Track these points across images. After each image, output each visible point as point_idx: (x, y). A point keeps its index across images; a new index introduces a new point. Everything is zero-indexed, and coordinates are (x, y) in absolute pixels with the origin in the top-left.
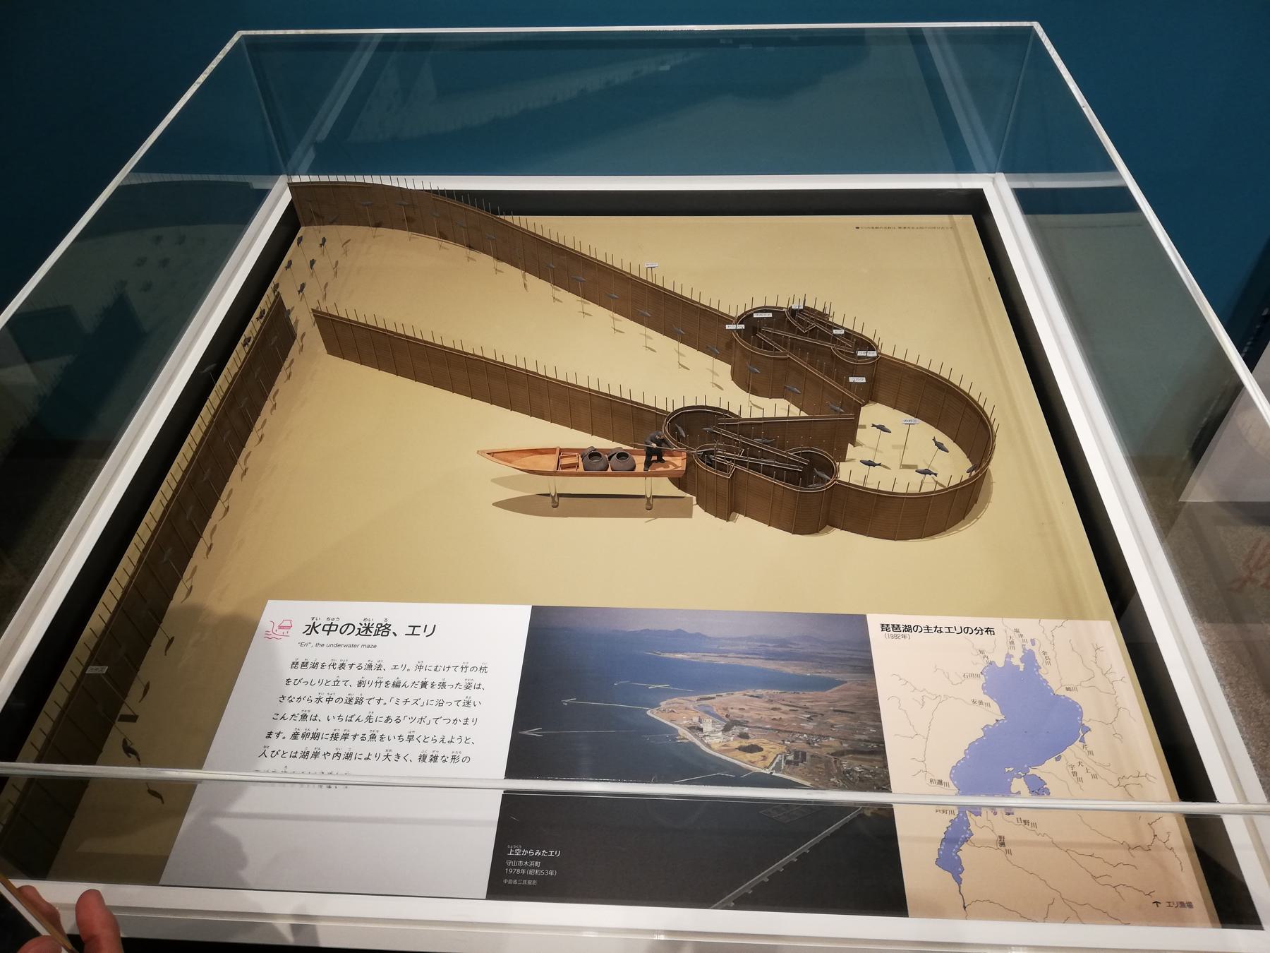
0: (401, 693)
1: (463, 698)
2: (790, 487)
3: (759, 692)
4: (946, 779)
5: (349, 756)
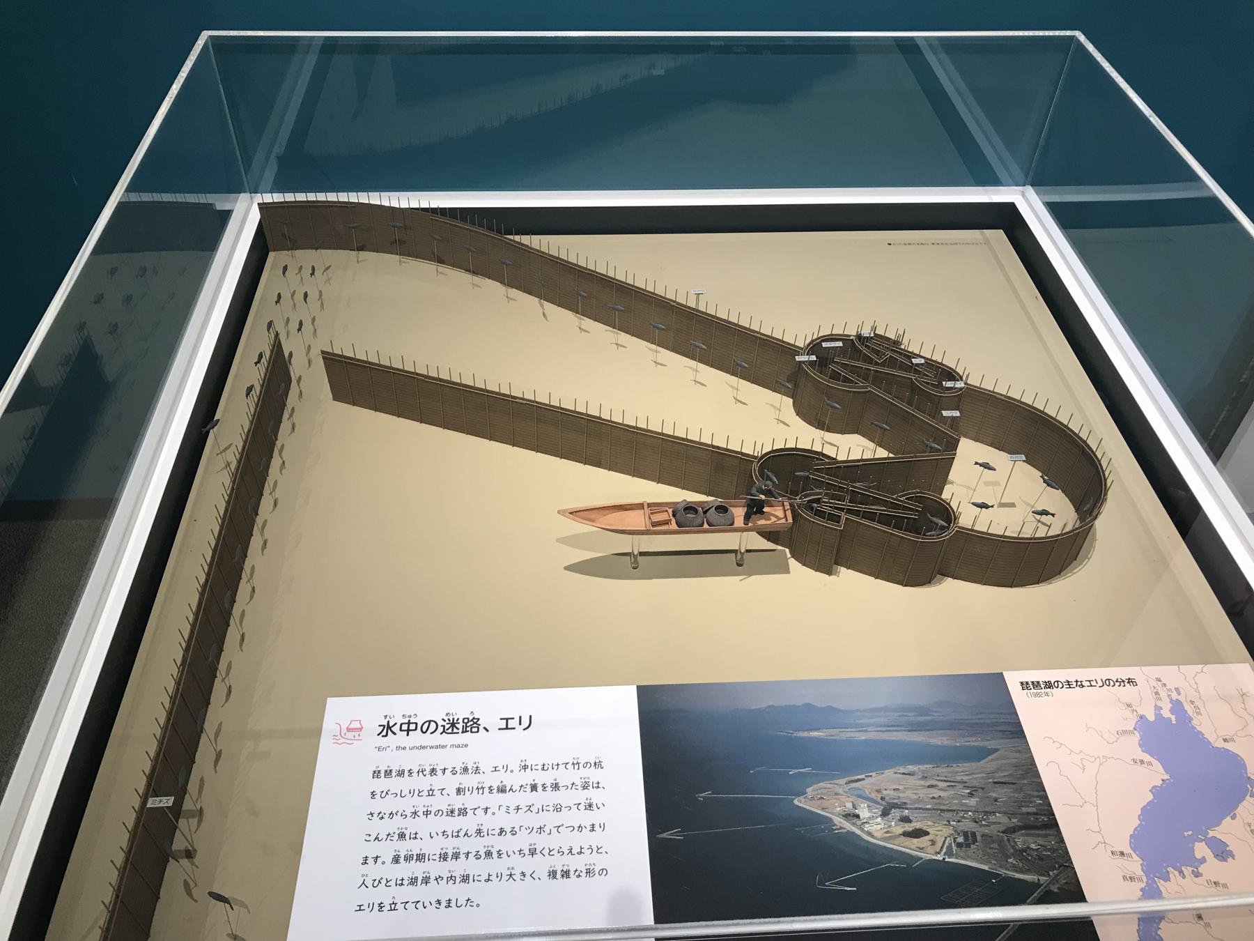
0: (509, 799)
1: (583, 801)
2: (911, 537)
3: (911, 768)
4: (1127, 850)
5: (465, 879)
